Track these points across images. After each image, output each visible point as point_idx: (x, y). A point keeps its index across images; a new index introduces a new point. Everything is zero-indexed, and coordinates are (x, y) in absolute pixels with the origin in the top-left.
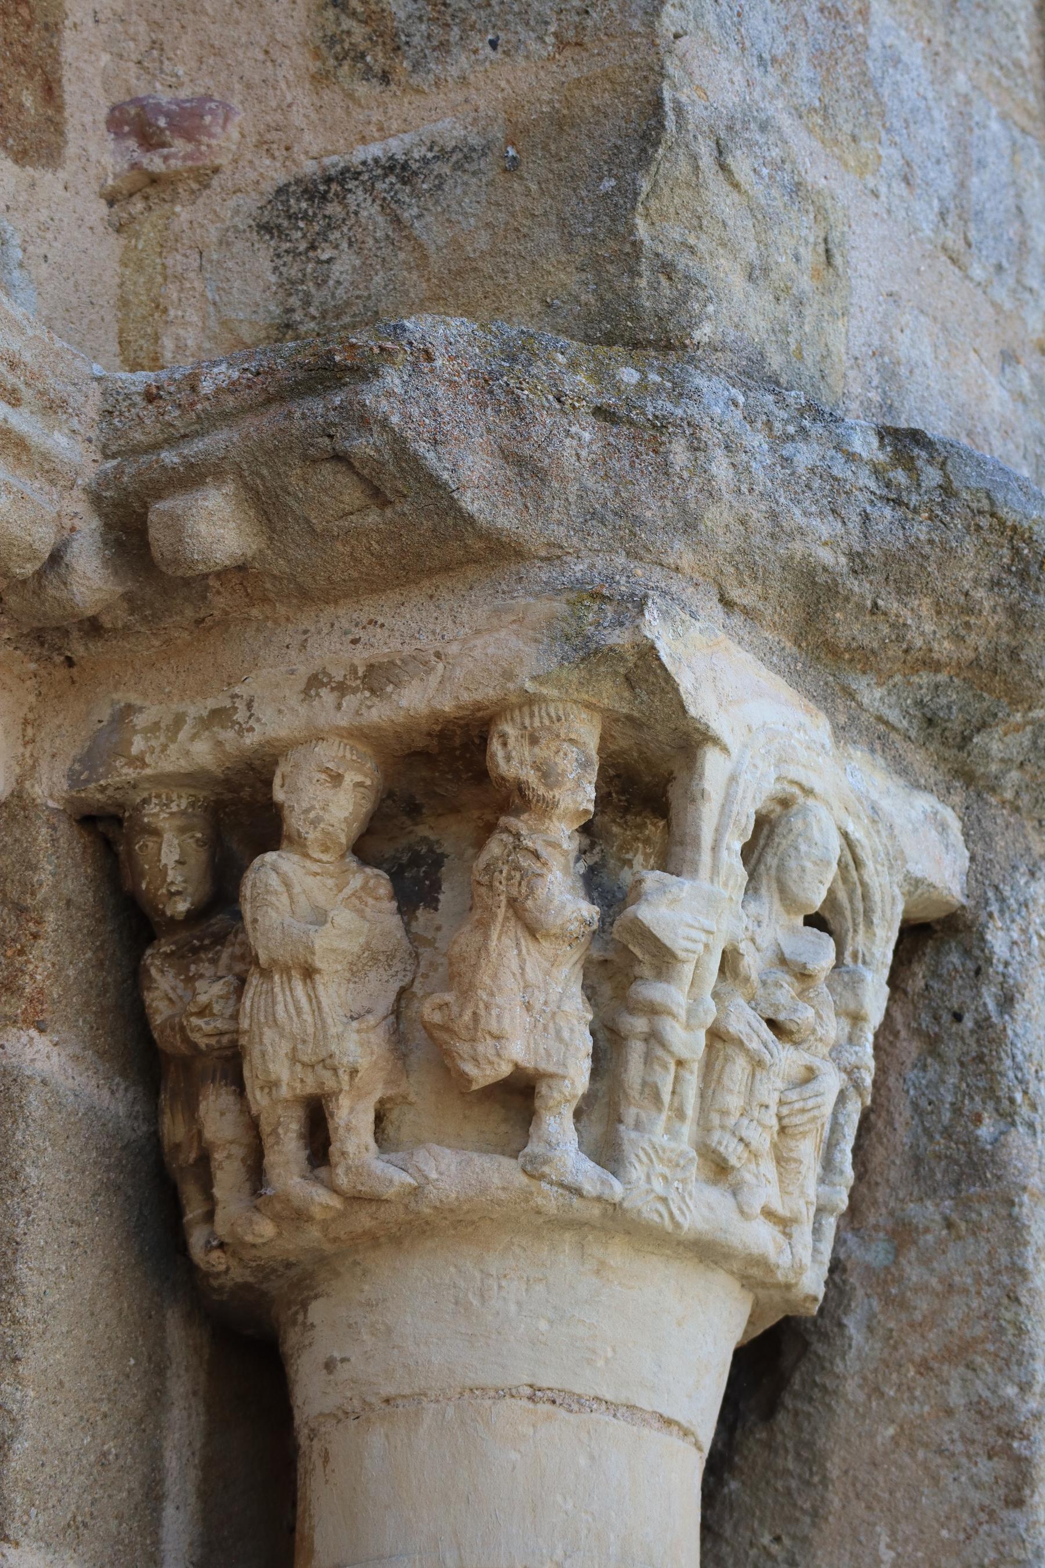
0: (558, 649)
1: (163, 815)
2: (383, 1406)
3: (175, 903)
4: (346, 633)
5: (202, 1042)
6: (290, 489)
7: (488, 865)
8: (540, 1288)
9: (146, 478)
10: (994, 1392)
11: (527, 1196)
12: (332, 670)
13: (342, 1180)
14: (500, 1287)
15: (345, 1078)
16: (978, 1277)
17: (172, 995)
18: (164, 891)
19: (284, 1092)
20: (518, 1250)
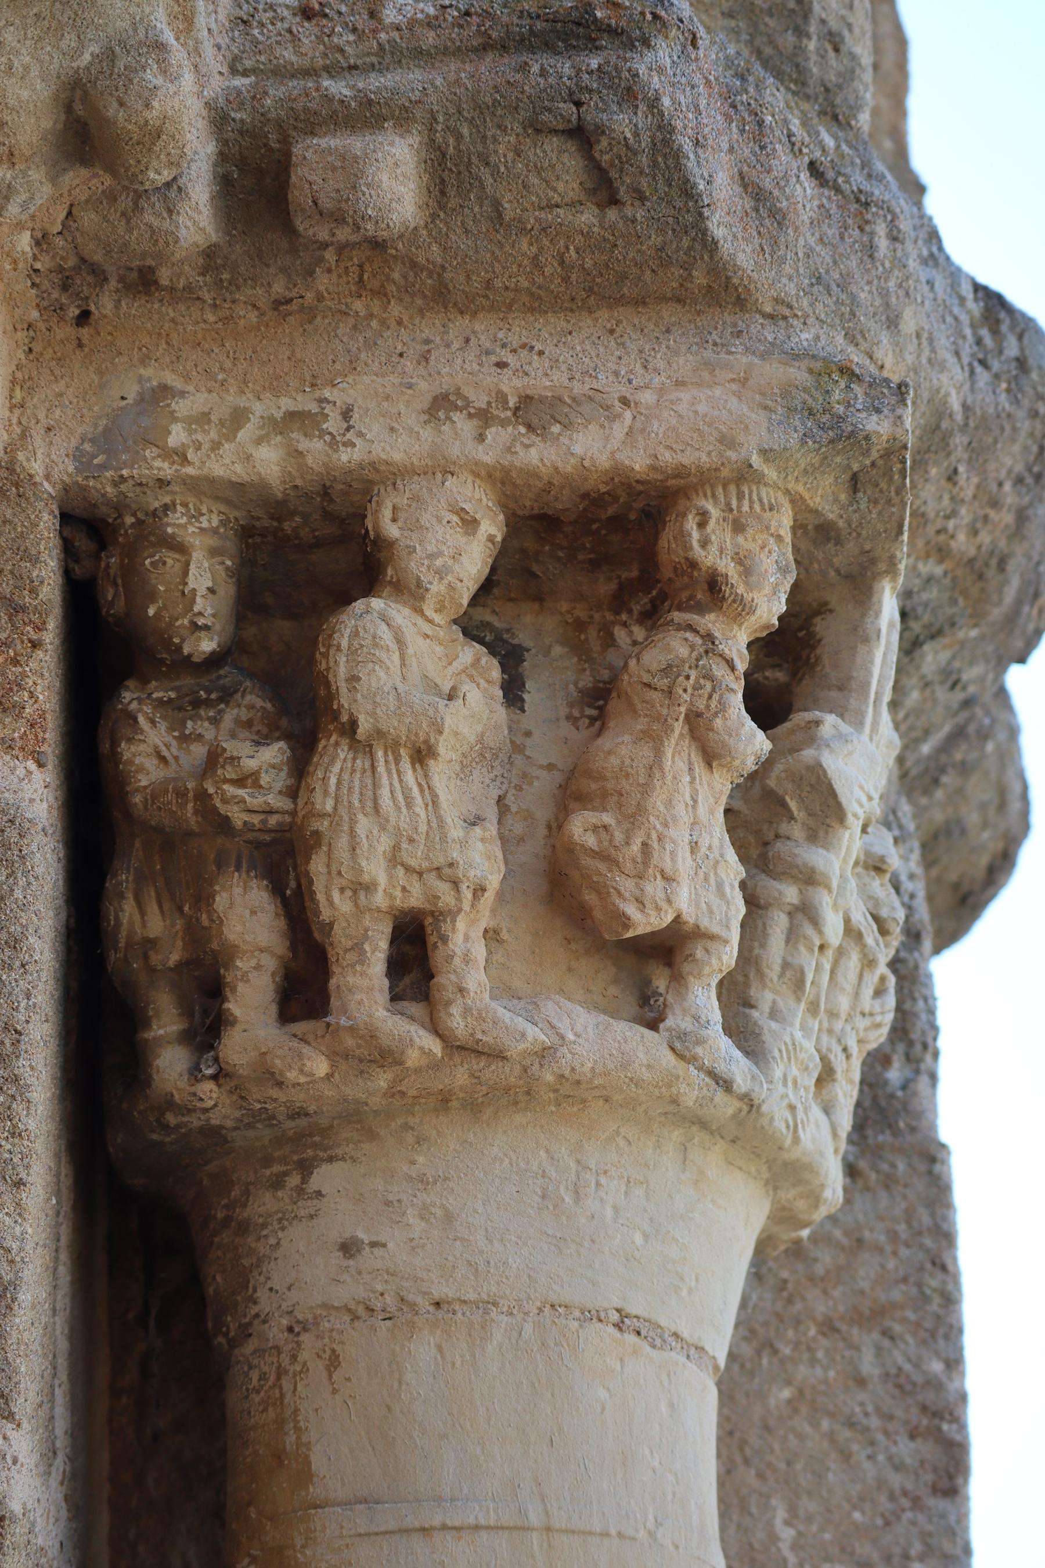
0: (797, 423)
1: (191, 529)
2: (431, 1309)
3: (199, 639)
4: (488, 353)
5: (238, 818)
6: (493, 159)
7: (670, 666)
8: (639, 1192)
9: (299, 105)
10: (917, 1366)
11: (672, 1079)
12: (470, 393)
13: (457, 1022)
14: (598, 1184)
15: (468, 895)
16: (893, 1236)
17: (165, 753)
18: (186, 622)
19: (380, 899)
20: (622, 1143)
